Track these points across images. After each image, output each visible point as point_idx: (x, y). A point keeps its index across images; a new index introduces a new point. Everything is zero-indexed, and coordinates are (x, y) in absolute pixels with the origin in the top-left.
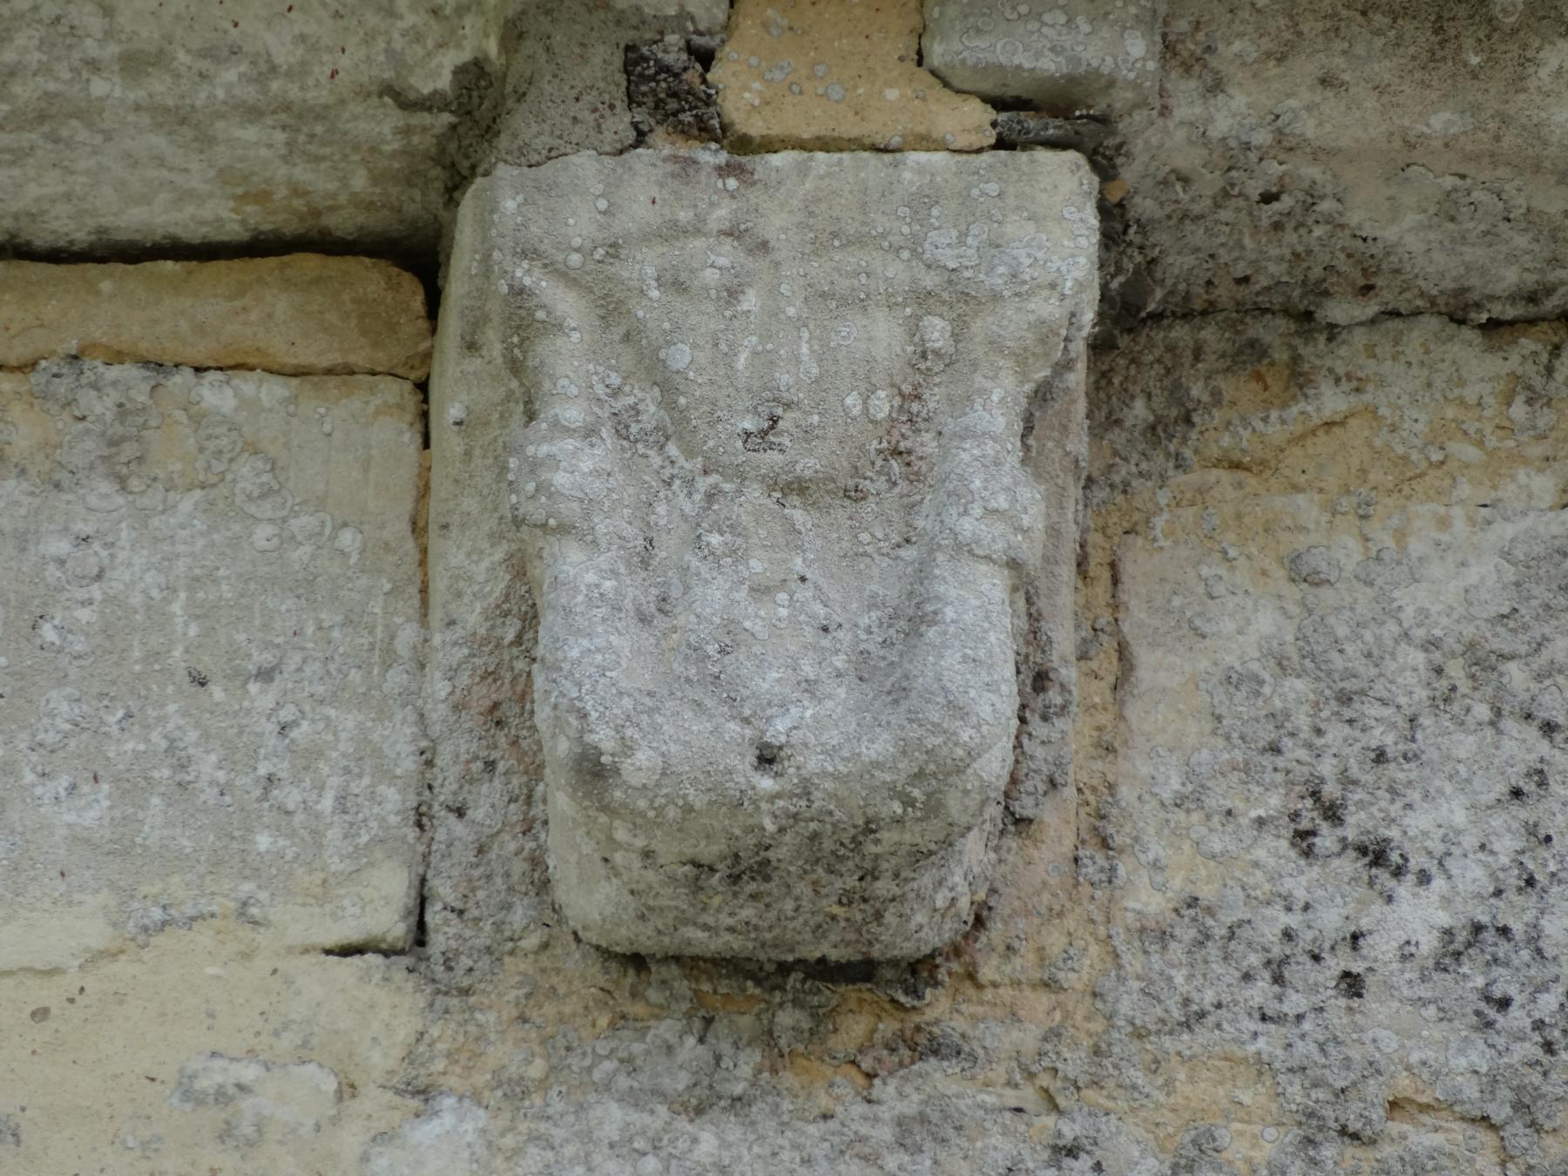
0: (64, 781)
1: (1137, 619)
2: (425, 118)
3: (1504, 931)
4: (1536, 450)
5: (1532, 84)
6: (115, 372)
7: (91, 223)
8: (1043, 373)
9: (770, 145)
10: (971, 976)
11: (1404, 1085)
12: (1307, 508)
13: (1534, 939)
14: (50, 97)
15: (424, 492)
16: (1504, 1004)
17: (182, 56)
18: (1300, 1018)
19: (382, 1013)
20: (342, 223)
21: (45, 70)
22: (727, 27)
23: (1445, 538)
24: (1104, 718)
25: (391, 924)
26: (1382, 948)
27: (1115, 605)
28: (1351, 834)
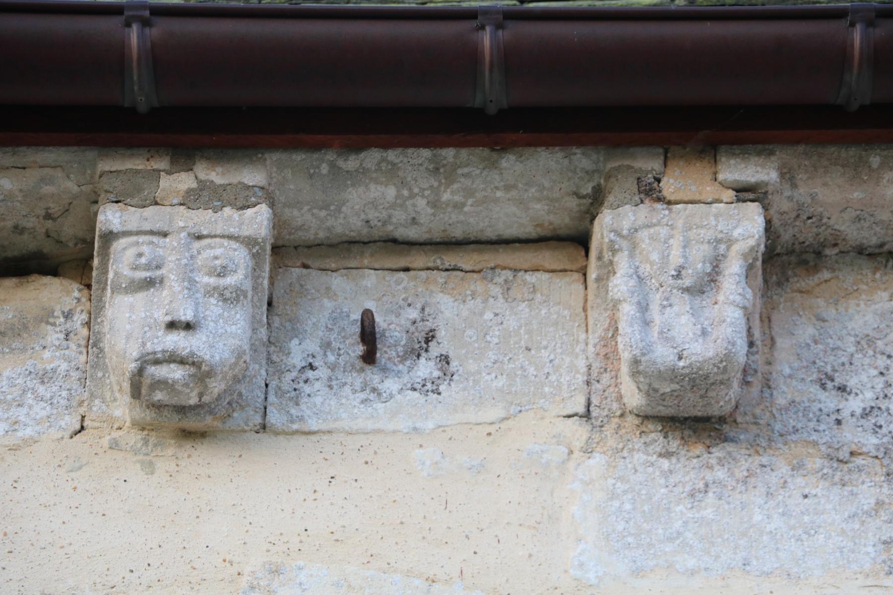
0: (493, 375)
1: (776, 330)
2: (584, 201)
3: (879, 408)
4: (883, 286)
5: (881, 184)
6: (504, 272)
7: (496, 233)
8: (751, 261)
9: (677, 203)
10: (735, 421)
11: (854, 448)
12: (821, 302)
13: (888, 409)
14: (485, 197)
15: (586, 301)
16: (881, 427)
17: (520, 185)
18: (824, 431)
19: (578, 432)
20: (563, 232)
21: (484, 190)
22: (664, 173)
23: (858, 309)
24: (768, 356)
25: (581, 410)
26: (845, 414)
27: (770, 327)
28: (836, 384)
